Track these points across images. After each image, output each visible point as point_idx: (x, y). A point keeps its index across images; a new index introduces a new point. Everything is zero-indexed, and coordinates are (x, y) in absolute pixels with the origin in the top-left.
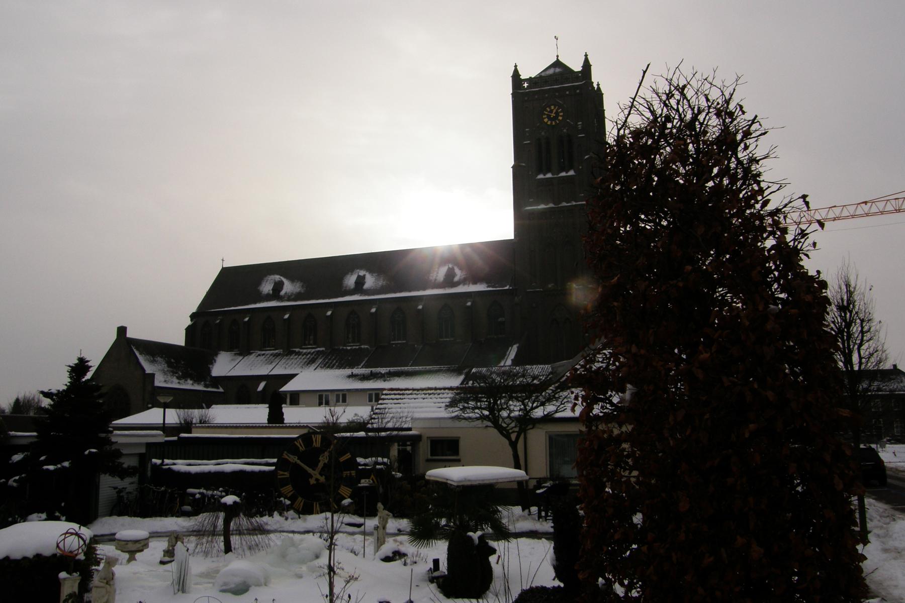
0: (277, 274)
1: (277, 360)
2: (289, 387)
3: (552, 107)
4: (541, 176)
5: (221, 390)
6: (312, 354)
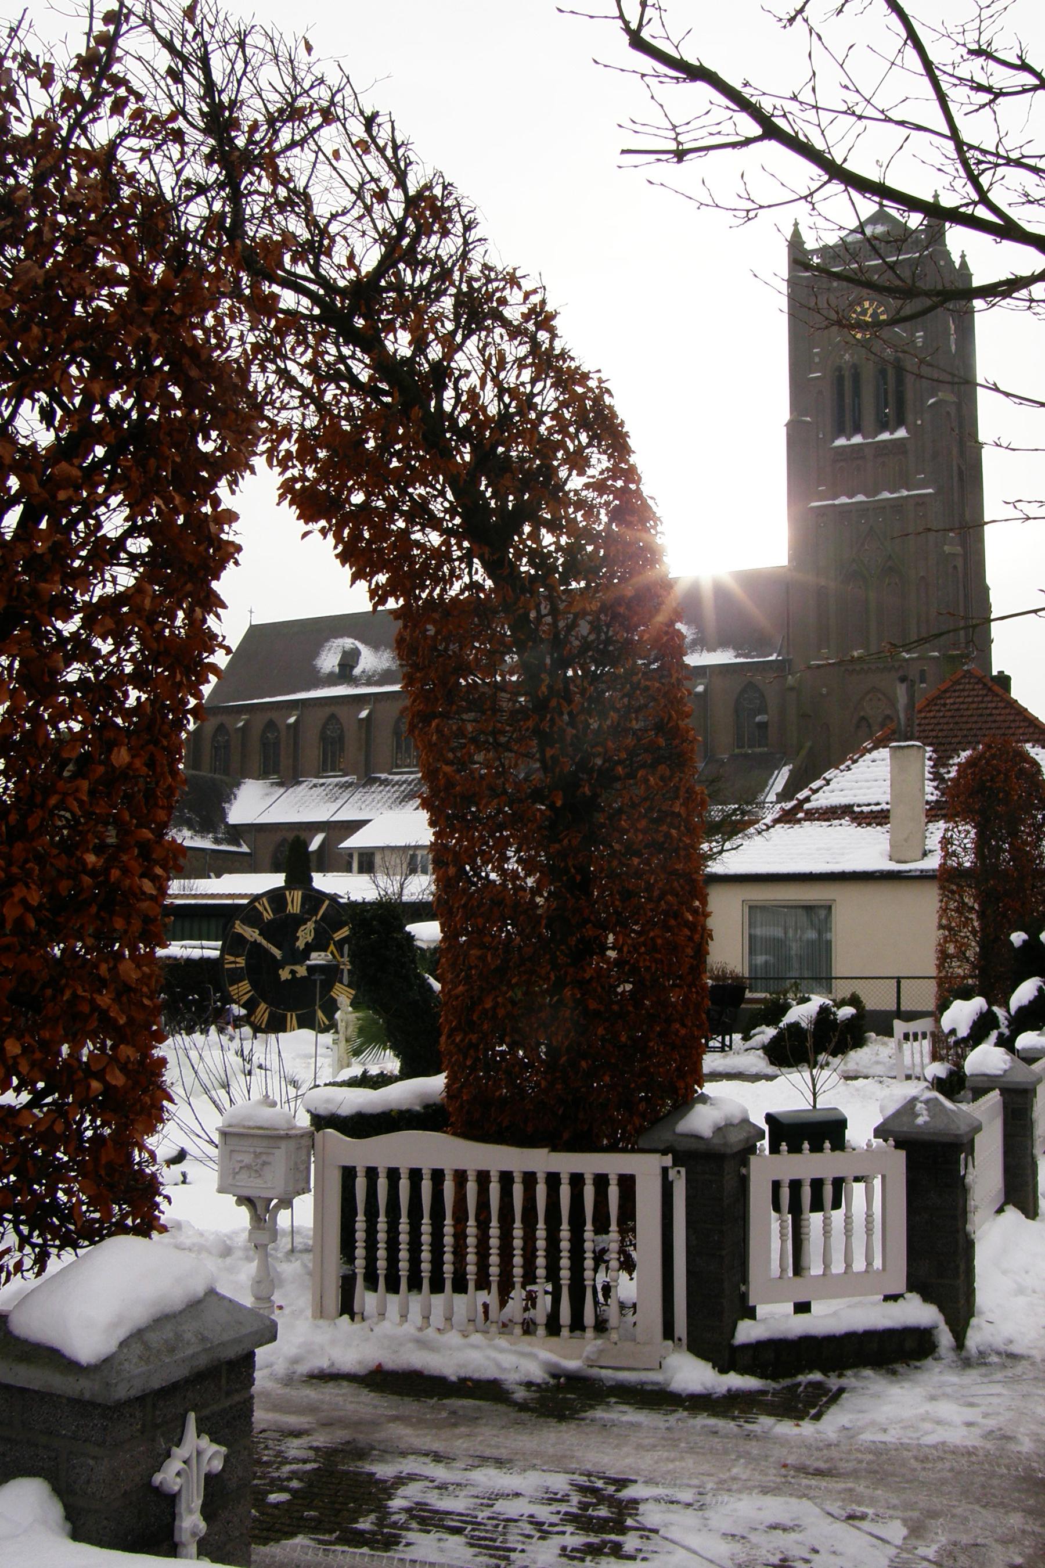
0: (349, 636)
1: (346, 795)
2: (355, 841)
3: (867, 304)
4: (841, 442)
5: (245, 849)
6: (410, 784)
